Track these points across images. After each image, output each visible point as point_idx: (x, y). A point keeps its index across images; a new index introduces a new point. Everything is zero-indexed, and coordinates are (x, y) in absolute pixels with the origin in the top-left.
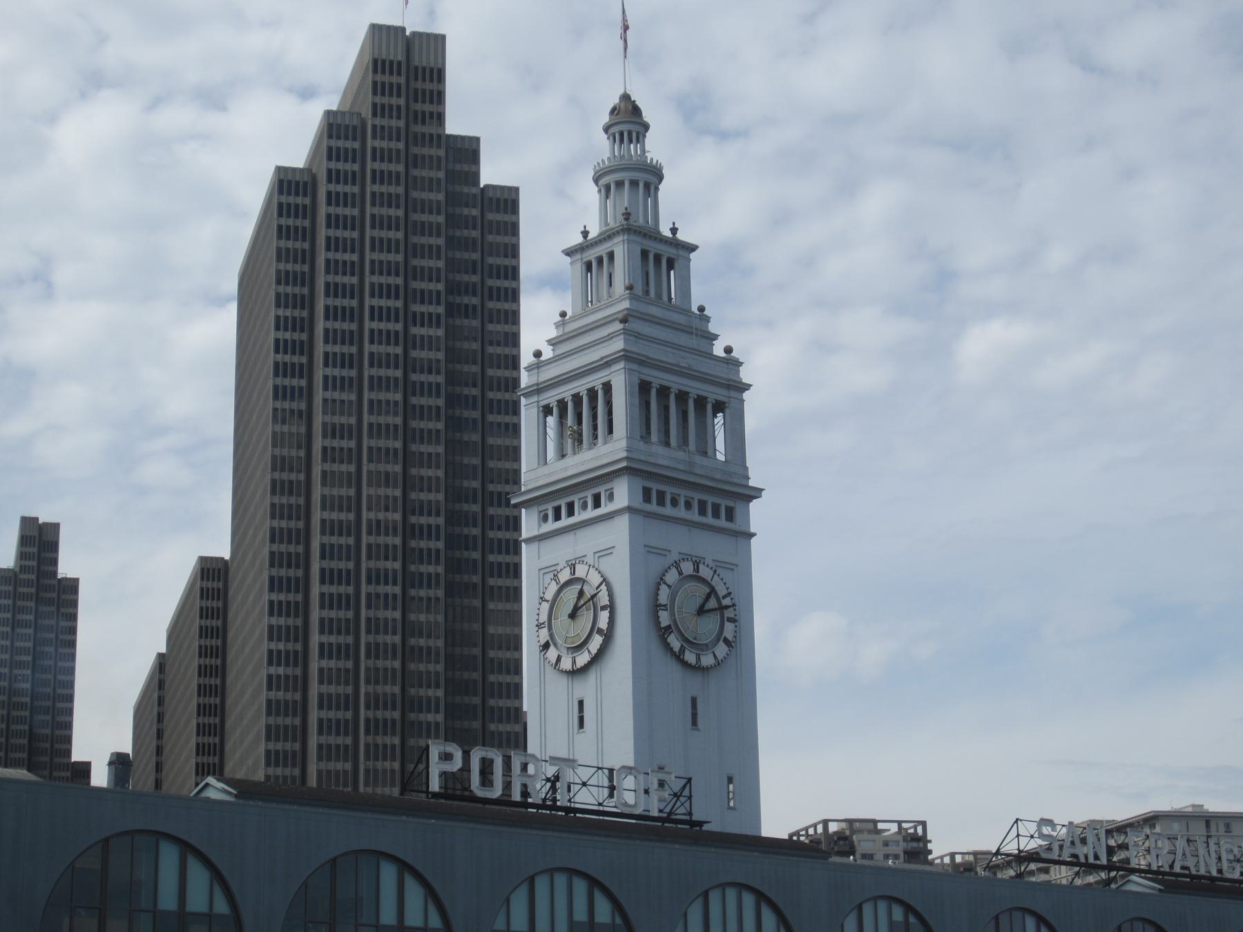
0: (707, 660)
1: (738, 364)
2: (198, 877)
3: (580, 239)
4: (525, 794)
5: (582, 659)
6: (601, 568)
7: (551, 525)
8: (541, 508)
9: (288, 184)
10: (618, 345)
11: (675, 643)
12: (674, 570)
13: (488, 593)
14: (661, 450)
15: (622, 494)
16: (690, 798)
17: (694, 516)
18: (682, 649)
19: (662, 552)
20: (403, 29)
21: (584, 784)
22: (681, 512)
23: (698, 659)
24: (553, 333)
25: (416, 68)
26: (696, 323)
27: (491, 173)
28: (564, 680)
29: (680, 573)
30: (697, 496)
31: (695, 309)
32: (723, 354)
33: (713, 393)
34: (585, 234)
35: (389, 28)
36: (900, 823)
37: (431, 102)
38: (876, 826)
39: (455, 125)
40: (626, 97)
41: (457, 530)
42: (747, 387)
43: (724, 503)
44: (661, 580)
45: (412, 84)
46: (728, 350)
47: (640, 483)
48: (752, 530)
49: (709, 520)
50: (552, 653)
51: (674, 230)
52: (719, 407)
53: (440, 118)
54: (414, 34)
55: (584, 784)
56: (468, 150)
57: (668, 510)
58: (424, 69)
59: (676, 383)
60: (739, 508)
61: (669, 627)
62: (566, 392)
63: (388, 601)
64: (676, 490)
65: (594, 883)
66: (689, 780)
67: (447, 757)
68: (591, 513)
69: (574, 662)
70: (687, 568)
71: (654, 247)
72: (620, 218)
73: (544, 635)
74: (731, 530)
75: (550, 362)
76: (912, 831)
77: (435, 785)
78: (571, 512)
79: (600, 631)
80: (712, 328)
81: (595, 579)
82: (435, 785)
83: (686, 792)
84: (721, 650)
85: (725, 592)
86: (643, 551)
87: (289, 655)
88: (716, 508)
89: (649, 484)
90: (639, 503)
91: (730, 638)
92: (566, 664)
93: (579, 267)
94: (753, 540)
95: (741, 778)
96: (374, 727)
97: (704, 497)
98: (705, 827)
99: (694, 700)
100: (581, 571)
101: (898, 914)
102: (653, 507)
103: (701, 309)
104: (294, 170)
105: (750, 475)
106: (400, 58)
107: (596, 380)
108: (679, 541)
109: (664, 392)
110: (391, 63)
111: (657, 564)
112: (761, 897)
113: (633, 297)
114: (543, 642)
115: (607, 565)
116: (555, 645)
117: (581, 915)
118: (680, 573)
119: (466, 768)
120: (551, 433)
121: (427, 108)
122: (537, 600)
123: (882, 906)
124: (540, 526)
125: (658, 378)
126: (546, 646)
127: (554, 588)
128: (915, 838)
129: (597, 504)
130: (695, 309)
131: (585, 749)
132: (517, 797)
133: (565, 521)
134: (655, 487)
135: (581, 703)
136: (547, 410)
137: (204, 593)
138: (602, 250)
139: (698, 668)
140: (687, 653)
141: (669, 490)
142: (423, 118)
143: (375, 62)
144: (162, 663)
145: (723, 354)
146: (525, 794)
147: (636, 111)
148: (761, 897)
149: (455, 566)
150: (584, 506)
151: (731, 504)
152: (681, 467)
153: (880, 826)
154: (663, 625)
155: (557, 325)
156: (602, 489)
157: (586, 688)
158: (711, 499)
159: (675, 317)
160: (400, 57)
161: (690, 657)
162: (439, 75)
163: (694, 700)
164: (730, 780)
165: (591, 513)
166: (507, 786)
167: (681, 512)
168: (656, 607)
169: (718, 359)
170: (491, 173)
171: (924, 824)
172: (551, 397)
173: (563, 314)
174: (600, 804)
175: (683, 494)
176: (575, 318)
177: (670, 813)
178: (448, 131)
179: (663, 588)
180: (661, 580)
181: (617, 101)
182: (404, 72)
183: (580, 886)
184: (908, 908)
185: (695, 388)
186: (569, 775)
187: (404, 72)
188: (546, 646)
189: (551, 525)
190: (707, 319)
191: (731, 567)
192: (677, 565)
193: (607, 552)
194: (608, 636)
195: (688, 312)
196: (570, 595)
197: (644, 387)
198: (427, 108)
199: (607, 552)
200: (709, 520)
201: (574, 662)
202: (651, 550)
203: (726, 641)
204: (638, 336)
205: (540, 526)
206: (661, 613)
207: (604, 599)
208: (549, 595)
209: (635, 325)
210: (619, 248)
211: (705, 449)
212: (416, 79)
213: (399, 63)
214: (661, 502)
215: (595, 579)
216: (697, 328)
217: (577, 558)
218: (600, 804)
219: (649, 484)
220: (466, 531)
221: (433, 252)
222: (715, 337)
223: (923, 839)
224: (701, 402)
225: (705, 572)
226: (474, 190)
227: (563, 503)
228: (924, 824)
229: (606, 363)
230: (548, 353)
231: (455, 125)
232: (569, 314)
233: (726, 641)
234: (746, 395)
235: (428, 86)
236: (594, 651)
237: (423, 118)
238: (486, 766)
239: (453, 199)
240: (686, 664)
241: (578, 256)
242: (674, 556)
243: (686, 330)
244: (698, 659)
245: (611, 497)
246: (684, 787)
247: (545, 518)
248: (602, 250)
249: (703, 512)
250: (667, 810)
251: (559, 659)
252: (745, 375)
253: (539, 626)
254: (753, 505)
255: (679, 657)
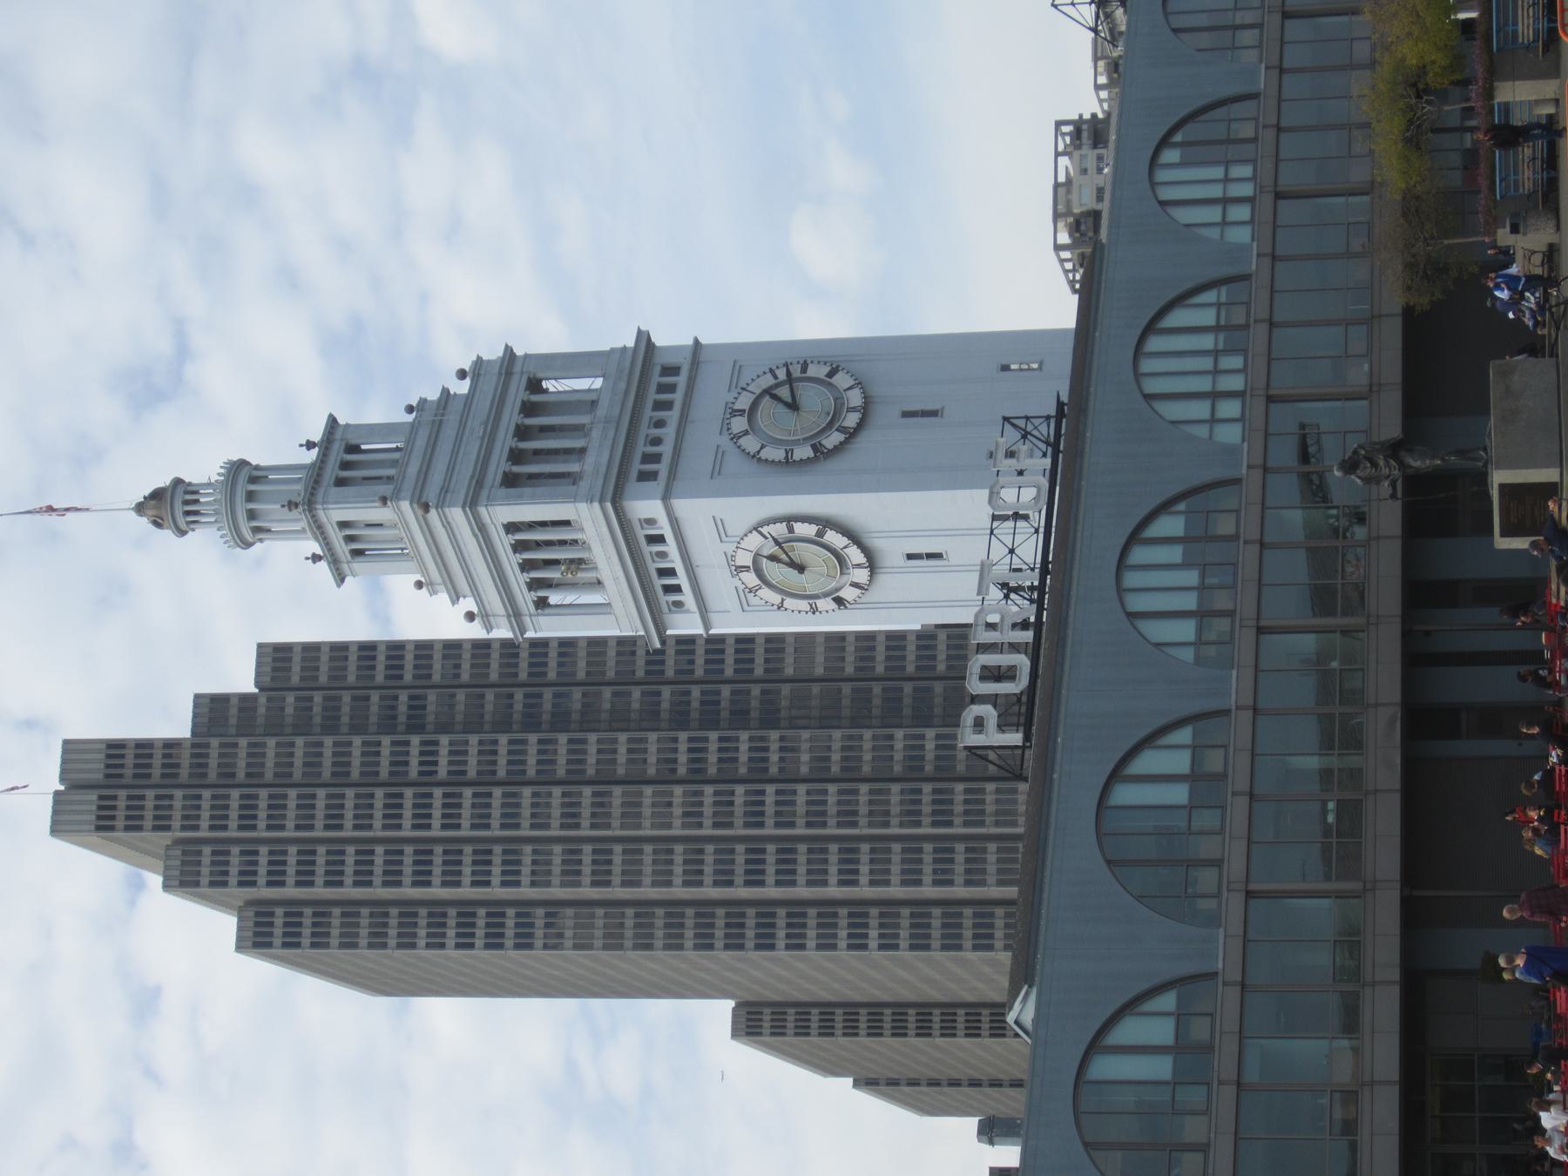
0: (855, 398)
1: (479, 362)
2: (1130, 1031)
3: (323, 565)
4: (1024, 625)
5: (855, 555)
6: (741, 533)
7: (687, 597)
8: (665, 608)
9: (259, 935)
10: (457, 515)
11: (834, 439)
12: (742, 441)
13: (774, 675)
14: (590, 459)
15: (646, 507)
16: (1027, 418)
17: (673, 416)
18: (842, 430)
19: (719, 456)
20: (57, 793)
21: (1012, 551)
22: (669, 433)
23: (854, 409)
24: (443, 597)
25: (107, 776)
26: (428, 416)
27: (241, 679)
28: (883, 579)
29: (746, 433)
30: (648, 413)
31: (410, 418)
32: (467, 382)
33: (518, 393)
34: (316, 558)
35: (55, 812)
36: (1057, 154)
37: (150, 756)
38: (1062, 185)
39: (177, 725)
40: (140, 508)
41: (695, 715)
42: (509, 351)
43: (656, 378)
44: (755, 457)
45: (128, 780)
46: (462, 374)
47: (633, 485)
48: (690, 342)
49: (678, 397)
50: (848, 593)
51: (310, 445)
52: (535, 385)
53: (171, 745)
54: (62, 780)
55: (1012, 551)
56: (213, 711)
57: (666, 449)
58: (108, 766)
59: (505, 440)
60: (661, 360)
61: (814, 447)
62: (518, 580)
63: (785, 801)
64: (641, 440)
65: (1135, 537)
66: (1006, 419)
67: (979, 724)
68: (671, 547)
69: (859, 566)
70: (739, 424)
71: (331, 471)
72: (295, 513)
73: (826, 604)
74: (691, 370)
75: (480, 601)
76: (1068, 139)
77: (1015, 738)
78: (671, 572)
79: (820, 534)
80: (433, 395)
81: (754, 541)
82: (1015, 738)
83: (1021, 423)
84: (842, 380)
85: (769, 376)
86: (718, 481)
87: (855, 923)
88: (663, 388)
89: (634, 474)
90: (658, 486)
91: (827, 369)
92: (862, 576)
93: (358, 565)
94: (703, 341)
95: (1003, 354)
96: (942, 816)
97: (649, 404)
98: (1065, 399)
99: (906, 414)
100: (745, 559)
101: (1171, 155)
102: (663, 468)
103: (410, 409)
104: (240, 929)
105: (620, 345)
106: (95, 797)
107: (503, 543)
108: (705, 436)
109: (516, 456)
110: (100, 808)
111: (734, 461)
112: (1150, 328)
113: (396, 496)
114: (834, 605)
115: (737, 526)
116: (838, 590)
117: (1174, 554)
118: (746, 433)
119: (993, 700)
120: (570, 598)
121: (157, 761)
122: (781, 613)
123: (1162, 175)
124: (688, 611)
125: (499, 464)
126: (840, 602)
127: (766, 593)
128: (1077, 134)
129: (660, 539)
130: (410, 418)
131: (968, 551)
132: (1028, 636)
133: (682, 579)
134: (636, 466)
135: (910, 557)
136: (542, 603)
137: (779, 1030)
138: (336, 537)
139: (866, 410)
140: (846, 424)
141: (641, 448)
142: (171, 767)
143: (99, 828)
144: (866, 1082)
145: (467, 382)
146: (1024, 625)
147: (157, 495)
148: (1150, 328)
149: (740, 717)
150: (663, 555)
151: (657, 370)
152: (611, 434)
153: (1062, 178)
154: (811, 454)
155: (433, 592)
156: (641, 534)
157: (892, 551)
158: (652, 396)
159: (421, 442)
160: (93, 796)
161: (851, 420)
162: (114, 749)
163: (906, 414)
164: (1005, 368)
165: (671, 547)
166: (1014, 647)
167: (669, 433)
168: (788, 462)
169: (473, 388)
170: (241, 679)
171: (1059, 124)
172: (526, 599)
173: (419, 585)
174: (1037, 531)
175: (645, 430)
176: (424, 570)
177: (1047, 443)
178: (188, 734)
179: (764, 454)
180: (755, 457)
181: (145, 520)
182: (114, 791)
183: (1139, 555)
184: (1164, 142)
185: (511, 416)
186: (1001, 570)
187: (114, 791)
188: (840, 602)
189: (687, 597)
190: (423, 401)
191: (737, 369)
192: (735, 438)
193: (720, 526)
194: (825, 523)
195: (413, 426)
196: (775, 571)
197: (510, 481)
198: (157, 761)
199: (720, 526)
200: (678, 397)
201: (859, 566)
202: (716, 471)
203: (831, 374)
204: (445, 490)
205: (688, 611)
206: (797, 456)
207: (779, 530)
208: (776, 598)
209: (431, 494)
210: (333, 514)
211: (588, 403)
212: (121, 776)
213: (101, 798)
214: (656, 458)
215: (754, 541)
216: (434, 416)
217: (727, 564)
218: (1037, 531)
219: (634, 474)
220: (695, 704)
221: (342, 751)
222: (445, 391)
223: (1078, 125)
224: (529, 409)
225: (744, 402)
226: (263, 700)
227: (659, 583)
228: (1059, 124)
229: (481, 529)
230: (469, 604)
231: (177, 725)
232: (419, 577)
233: (831, 374)
234: (519, 352)
235: (129, 760)
236: (845, 541)
237: (171, 767)
238: (993, 674)
239: (275, 726)
240: (861, 425)
241: (345, 567)
242: (725, 440)
243: (438, 427)
244: (854, 409)
245: (651, 522)
246: (1014, 425)
247: (679, 604)
248: (336, 537)
249: (667, 405)
250: (1043, 447)
251: (855, 585)
252: (493, 353)
253: (814, 610)
254: (659, 340)
255: (852, 434)
